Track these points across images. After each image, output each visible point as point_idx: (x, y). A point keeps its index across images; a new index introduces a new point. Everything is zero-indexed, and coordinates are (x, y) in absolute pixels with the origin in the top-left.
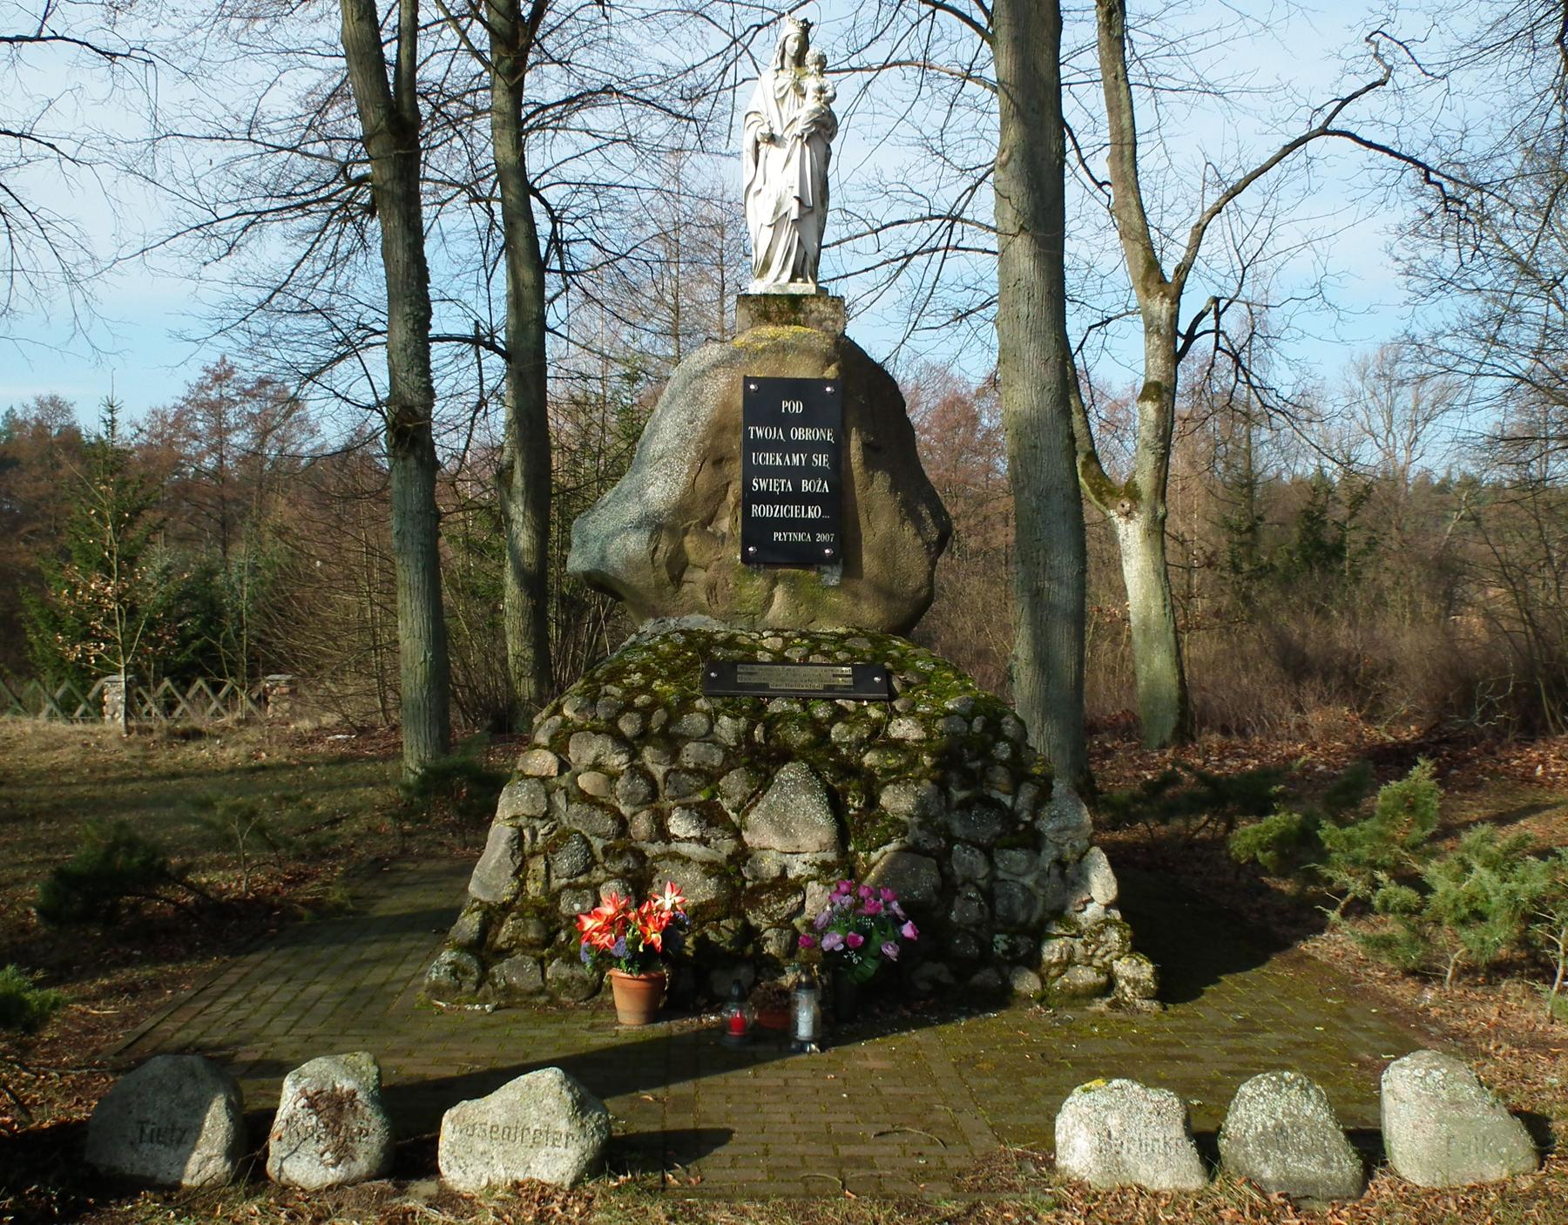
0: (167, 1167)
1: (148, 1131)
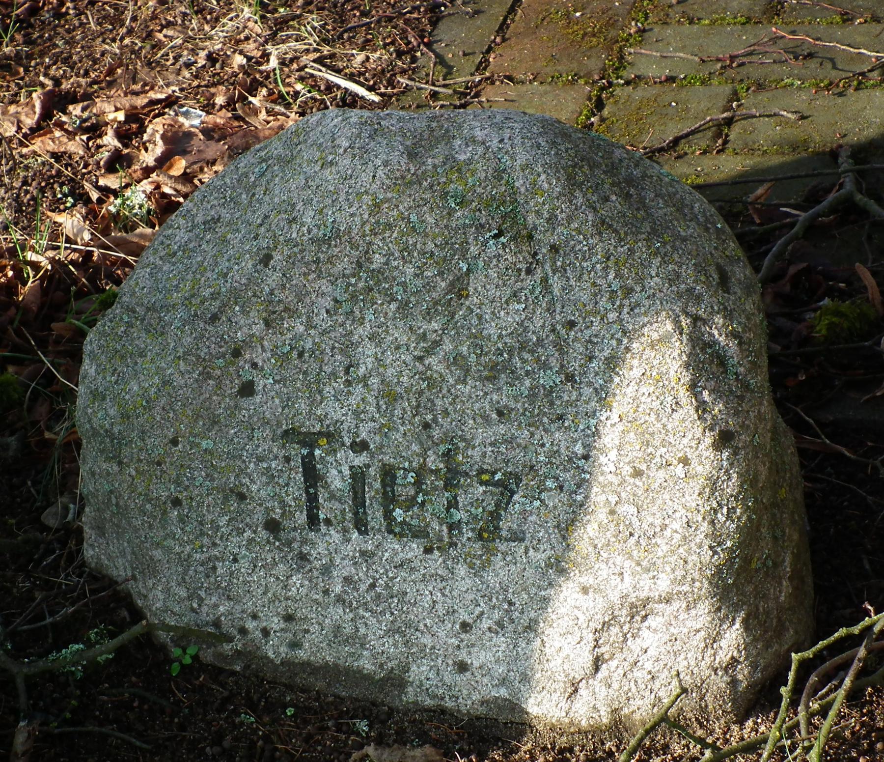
0: (446, 635)
1: (337, 479)
